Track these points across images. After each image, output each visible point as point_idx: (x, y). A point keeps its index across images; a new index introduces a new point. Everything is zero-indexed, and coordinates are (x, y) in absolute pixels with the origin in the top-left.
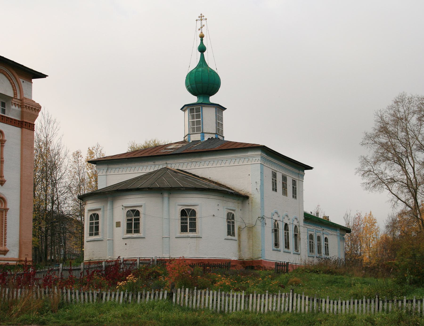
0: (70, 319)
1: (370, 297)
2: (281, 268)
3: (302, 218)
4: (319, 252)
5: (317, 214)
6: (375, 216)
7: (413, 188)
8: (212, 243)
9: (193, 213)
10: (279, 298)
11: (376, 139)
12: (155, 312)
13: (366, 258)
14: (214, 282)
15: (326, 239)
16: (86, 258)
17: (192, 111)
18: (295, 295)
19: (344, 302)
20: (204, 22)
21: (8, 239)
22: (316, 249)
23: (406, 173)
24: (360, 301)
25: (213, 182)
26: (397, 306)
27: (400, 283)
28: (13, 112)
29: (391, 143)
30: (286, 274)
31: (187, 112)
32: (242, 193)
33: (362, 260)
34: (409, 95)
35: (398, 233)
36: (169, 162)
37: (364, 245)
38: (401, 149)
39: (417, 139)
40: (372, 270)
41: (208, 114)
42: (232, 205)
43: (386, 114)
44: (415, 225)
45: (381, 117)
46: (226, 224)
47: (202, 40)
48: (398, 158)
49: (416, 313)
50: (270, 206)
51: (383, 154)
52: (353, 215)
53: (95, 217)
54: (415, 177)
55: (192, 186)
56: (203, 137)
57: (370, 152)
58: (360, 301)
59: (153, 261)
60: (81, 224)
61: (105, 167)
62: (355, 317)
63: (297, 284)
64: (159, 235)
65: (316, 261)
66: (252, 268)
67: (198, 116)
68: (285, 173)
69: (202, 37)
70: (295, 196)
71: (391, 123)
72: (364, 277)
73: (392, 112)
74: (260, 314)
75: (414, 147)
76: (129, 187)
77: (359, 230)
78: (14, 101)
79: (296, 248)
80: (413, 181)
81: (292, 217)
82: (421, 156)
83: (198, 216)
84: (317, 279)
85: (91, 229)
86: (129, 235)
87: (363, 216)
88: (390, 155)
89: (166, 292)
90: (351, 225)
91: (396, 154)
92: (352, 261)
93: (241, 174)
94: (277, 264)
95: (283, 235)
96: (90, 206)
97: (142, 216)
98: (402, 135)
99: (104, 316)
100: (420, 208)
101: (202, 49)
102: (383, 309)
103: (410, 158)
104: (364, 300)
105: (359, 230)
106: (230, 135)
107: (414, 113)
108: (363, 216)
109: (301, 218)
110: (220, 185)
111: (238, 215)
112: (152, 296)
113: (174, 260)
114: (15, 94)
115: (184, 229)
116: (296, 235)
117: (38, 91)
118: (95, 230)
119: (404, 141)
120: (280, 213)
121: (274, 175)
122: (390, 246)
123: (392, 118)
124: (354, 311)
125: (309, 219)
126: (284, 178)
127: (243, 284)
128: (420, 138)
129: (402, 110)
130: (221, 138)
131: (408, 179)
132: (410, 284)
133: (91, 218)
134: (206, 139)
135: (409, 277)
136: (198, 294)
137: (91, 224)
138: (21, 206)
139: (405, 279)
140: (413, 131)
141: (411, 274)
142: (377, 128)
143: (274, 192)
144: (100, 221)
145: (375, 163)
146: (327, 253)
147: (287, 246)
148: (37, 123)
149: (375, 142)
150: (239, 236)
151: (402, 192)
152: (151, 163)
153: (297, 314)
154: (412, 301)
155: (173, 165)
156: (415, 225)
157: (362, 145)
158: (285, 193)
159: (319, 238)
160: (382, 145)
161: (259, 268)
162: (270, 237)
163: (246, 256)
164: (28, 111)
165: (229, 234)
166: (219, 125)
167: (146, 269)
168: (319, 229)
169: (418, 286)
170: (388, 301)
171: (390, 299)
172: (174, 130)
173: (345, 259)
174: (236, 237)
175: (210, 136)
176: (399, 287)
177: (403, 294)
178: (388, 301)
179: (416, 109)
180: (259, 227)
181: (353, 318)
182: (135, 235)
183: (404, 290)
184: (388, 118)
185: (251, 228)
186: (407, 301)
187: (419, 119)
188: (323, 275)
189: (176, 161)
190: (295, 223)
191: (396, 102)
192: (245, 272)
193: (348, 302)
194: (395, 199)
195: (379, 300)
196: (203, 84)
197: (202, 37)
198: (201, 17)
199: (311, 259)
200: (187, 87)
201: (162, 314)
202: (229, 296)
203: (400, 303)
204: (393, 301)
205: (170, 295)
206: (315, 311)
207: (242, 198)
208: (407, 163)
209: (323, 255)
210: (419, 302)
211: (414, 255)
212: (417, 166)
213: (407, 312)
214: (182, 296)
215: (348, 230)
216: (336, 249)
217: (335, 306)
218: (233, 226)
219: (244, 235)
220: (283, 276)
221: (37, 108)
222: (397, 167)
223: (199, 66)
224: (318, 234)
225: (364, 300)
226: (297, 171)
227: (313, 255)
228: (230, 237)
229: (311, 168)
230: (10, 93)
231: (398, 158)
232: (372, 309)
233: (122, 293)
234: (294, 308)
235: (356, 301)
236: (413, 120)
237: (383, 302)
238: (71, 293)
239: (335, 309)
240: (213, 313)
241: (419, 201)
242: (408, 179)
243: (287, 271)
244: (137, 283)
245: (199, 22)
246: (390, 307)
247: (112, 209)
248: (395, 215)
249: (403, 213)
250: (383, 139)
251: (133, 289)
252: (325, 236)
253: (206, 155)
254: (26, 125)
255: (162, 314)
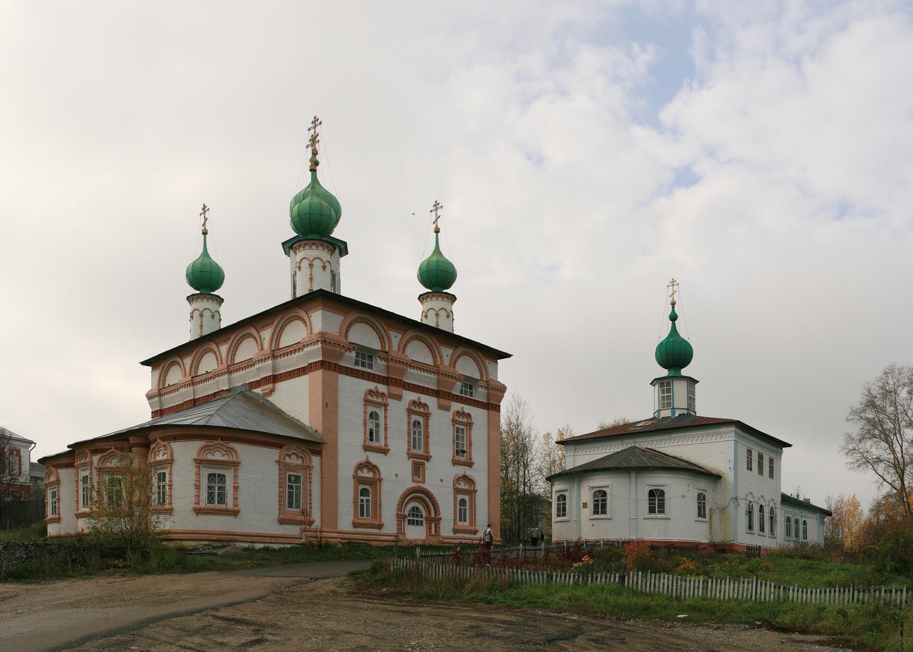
0: (516, 599)
1: (844, 586)
2: (753, 552)
3: (779, 499)
4: (797, 535)
5: (798, 496)
6: (858, 499)
7: (899, 468)
8: (681, 524)
9: (662, 493)
10: (741, 585)
11: (862, 415)
12: (604, 595)
13: (848, 543)
14: (678, 565)
15: (805, 523)
16: (554, 539)
17: (662, 385)
18: (759, 581)
19: (828, 590)
20: (676, 288)
21: (477, 520)
22: (793, 533)
23: (894, 452)
24: (833, 590)
25: (684, 461)
26: (874, 597)
27: (879, 571)
28: (480, 394)
29: (879, 418)
30: (758, 559)
31: (657, 387)
32: (714, 472)
33: (843, 545)
34: (899, 366)
35: (882, 517)
36: (637, 440)
37: (846, 530)
38: (889, 425)
39: (906, 414)
40: (851, 556)
41: (680, 388)
42: (703, 485)
43: (874, 386)
44: (901, 509)
45: (869, 390)
46: (697, 505)
47: (673, 308)
48: (886, 435)
49: (895, 605)
50: (745, 485)
51: (869, 432)
52: (835, 497)
53: (562, 498)
54: (902, 457)
55: (660, 465)
56: (674, 413)
57: (855, 429)
58: (833, 590)
59: (618, 542)
60: (550, 503)
61: (572, 447)
62: (825, 608)
63: (767, 569)
64: (626, 516)
65: (792, 545)
66: (724, 551)
67: (669, 391)
68: (762, 451)
69: (673, 304)
70: (771, 475)
71: (879, 396)
72: (842, 563)
73: (881, 384)
74: (719, 601)
75: (904, 423)
76: (596, 467)
77: (841, 513)
78: (481, 383)
79: (772, 530)
80: (901, 460)
81: (767, 498)
82: (910, 434)
83: (666, 496)
84: (791, 564)
85: (558, 509)
86: (596, 516)
87: (846, 499)
88: (877, 432)
89: (617, 575)
90: (833, 508)
91: (883, 431)
92: (832, 546)
93: (714, 452)
94: (749, 548)
95: (757, 516)
96: (558, 486)
97: (608, 496)
98: (890, 409)
99: (551, 598)
100: (907, 490)
101: (673, 318)
102: (858, 600)
103: (898, 436)
104: (837, 589)
105: (841, 513)
106: (703, 410)
107: (904, 385)
108: (846, 499)
109: (778, 499)
110: (691, 464)
111: (709, 496)
112: (603, 579)
113: (633, 541)
114: (482, 376)
115: (652, 510)
116: (772, 518)
117: (504, 371)
118: (562, 511)
119: (892, 416)
120: (755, 494)
121: (749, 452)
122: (873, 530)
123: (881, 391)
124: (825, 601)
125: (786, 500)
126: (761, 457)
127: (709, 568)
128: (910, 414)
129: (891, 382)
130: (693, 413)
131: (896, 458)
132: (890, 572)
133: (559, 499)
134: (677, 415)
135: (890, 564)
136: (651, 578)
137: (558, 505)
138: (489, 488)
139: (885, 566)
140: (903, 406)
141: (893, 560)
142: (864, 402)
143: (749, 472)
144: (567, 501)
145: (860, 441)
146: (805, 537)
147: (762, 529)
148: (504, 404)
149: (862, 418)
150: (711, 517)
151: (889, 473)
152: (620, 442)
153: (761, 603)
154: (891, 591)
155: (642, 444)
156: (901, 509)
157: (848, 420)
158: (761, 472)
159: (797, 521)
160: (868, 420)
161: (732, 551)
162: (743, 519)
163: (718, 539)
164: (494, 392)
165: (699, 515)
166: (691, 399)
167: (608, 550)
168: (797, 511)
169: (899, 575)
170: (864, 591)
171: (866, 590)
172: (642, 406)
173: (825, 544)
174: (707, 519)
175: (681, 412)
176: (877, 575)
177: (882, 583)
178: (864, 591)
179: (906, 380)
180: (732, 508)
181: (822, 609)
182: (602, 516)
183: (883, 579)
184: (876, 391)
185: (723, 510)
186: (885, 592)
187: (909, 393)
188: (797, 560)
189: (645, 439)
190: (772, 504)
191: (886, 373)
192: (715, 556)
193: (818, 590)
194: (881, 480)
195: (854, 589)
196: (675, 355)
197: (673, 304)
198: (673, 283)
199: (787, 543)
200: (657, 359)
201: (611, 599)
202: (686, 580)
203: (877, 592)
204: (869, 591)
205: (622, 579)
206: (782, 600)
207: (714, 477)
208: (895, 441)
209: (801, 540)
210: (899, 593)
211: (897, 540)
212: (905, 445)
213: (885, 603)
214: (635, 579)
215: (828, 513)
216: (815, 534)
217: (804, 595)
218: (704, 507)
219: (716, 517)
220: (754, 560)
221: (503, 389)
222: (884, 445)
223: (670, 336)
224: (796, 517)
225: (837, 589)
226: (775, 449)
227: (790, 539)
228: (700, 519)
229: (790, 446)
230: (477, 376)
231: (886, 435)
232: (846, 600)
233: (572, 575)
234: (758, 596)
235: (828, 590)
236: (903, 393)
237: (859, 592)
238: (522, 574)
239: (804, 598)
240: (668, 598)
241: (906, 483)
242: (896, 458)
243: (759, 555)
244: (593, 565)
245: (671, 288)
246: (866, 598)
247: (579, 489)
248: (880, 498)
249: (889, 495)
250: (870, 415)
251: (588, 571)
252: (804, 519)
253: (677, 432)
254: (493, 407)
255: (611, 599)
